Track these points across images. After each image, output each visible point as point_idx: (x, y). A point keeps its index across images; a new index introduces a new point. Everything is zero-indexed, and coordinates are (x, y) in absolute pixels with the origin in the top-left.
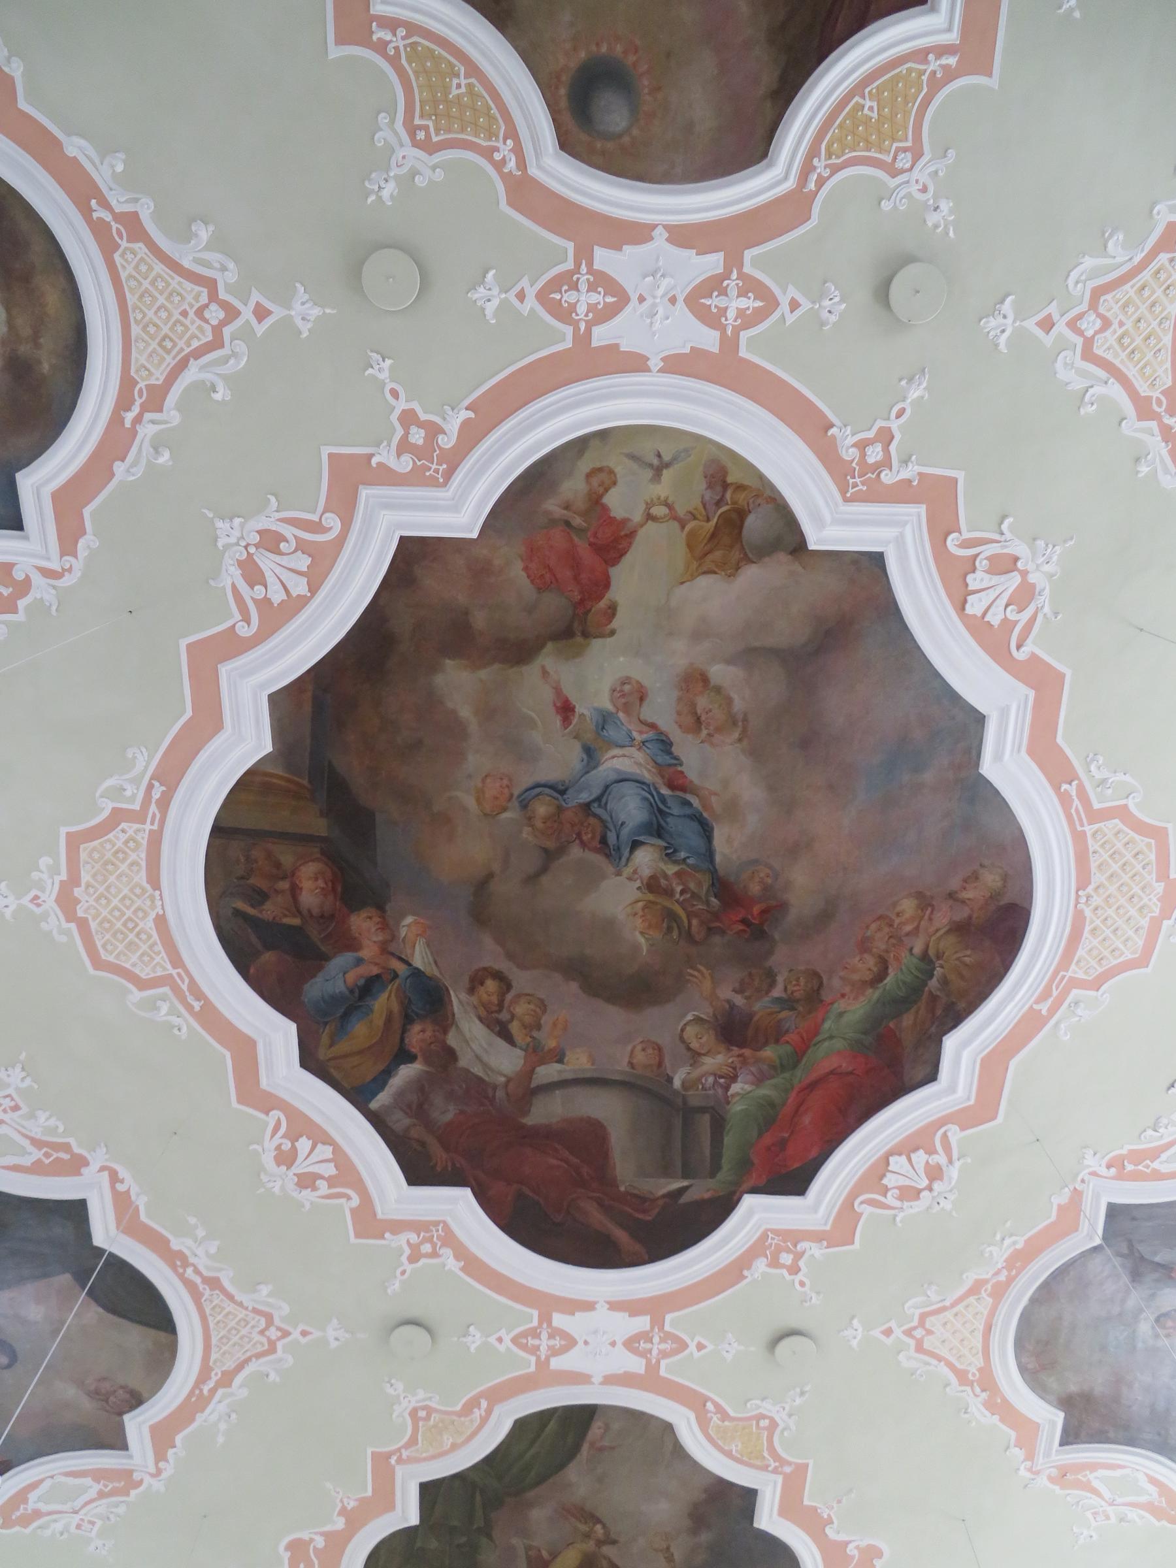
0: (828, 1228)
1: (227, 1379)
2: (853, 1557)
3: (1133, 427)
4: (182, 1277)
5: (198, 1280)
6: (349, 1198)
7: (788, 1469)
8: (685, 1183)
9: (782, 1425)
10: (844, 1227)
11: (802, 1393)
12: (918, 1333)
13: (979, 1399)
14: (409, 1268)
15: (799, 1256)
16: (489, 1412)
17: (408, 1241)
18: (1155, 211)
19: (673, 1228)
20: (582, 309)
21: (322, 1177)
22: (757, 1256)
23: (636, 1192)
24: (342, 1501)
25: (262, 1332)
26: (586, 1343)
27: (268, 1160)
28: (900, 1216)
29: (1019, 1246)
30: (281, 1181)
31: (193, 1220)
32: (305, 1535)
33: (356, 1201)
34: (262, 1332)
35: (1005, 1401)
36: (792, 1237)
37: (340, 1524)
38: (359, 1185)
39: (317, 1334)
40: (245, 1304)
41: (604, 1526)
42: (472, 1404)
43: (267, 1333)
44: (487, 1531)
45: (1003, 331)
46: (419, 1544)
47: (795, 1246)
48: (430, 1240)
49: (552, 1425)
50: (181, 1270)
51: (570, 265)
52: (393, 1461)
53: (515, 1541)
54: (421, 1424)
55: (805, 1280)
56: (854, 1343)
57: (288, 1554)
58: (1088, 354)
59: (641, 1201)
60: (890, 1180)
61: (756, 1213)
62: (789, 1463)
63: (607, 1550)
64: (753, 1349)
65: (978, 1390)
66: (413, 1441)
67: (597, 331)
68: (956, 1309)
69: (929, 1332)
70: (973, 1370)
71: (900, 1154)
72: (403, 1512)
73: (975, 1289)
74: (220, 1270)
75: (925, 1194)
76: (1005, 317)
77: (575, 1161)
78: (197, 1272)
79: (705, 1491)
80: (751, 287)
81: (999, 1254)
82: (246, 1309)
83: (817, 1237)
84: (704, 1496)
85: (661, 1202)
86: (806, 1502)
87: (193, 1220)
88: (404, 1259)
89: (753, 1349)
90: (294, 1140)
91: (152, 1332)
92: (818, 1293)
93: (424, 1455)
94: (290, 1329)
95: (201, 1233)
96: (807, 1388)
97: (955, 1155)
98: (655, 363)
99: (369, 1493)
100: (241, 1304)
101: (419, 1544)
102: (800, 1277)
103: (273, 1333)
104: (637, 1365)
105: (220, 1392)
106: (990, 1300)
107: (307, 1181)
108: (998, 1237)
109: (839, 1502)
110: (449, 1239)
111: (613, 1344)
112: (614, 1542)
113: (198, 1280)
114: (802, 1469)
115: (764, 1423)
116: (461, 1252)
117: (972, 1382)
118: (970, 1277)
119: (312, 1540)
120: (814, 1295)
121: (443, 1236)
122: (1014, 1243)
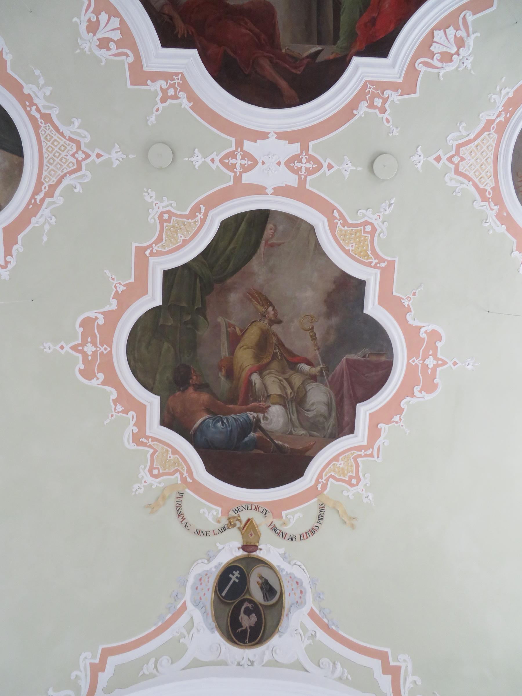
0: (401, 80)
1: (50, 194)
2: (424, 339)
3: (479, 204)
4: (28, 113)
5: (38, 116)
6: (128, 56)
7: (383, 265)
8: (319, 48)
9: (379, 230)
10: (409, 83)
11: (390, 205)
12: (456, 159)
13: (493, 212)
14: (161, 106)
15: (385, 101)
16: (206, 215)
17: (161, 87)
18: (481, 115)
19: (311, 82)
20: (238, 166)
21: (113, 41)
22: (360, 101)
23: (290, 53)
24: (116, 287)
25: (73, 155)
26: (263, 163)
27: (83, 28)
28: (442, 72)
29: (511, 95)
30: (88, 43)
31: (37, 72)
32: (92, 314)
33: (131, 59)
34: (73, 155)
35: (508, 214)
36: (382, 86)
37: (114, 305)
38: (134, 47)
39: (106, 156)
40: (65, 134)
41: (274, 309)
42: (196, 209)
43: (76, 155)
44: (202, 311)
45: (419, 162)
46: (161, 322)
47: (383, 94)
48: (173, 86)
49: (243, 226)
50: (28, 109)
51: (233, 148)
52: (147, 253)
53: (220, 319)
54: (165, 224)
55: (389, 118)
56: (419, 166)
57: (82, 329)
58: (457, 172)
59: (295, 59)
60: (435, 48)
61: (362, 70)
62: (384, 261)
63: (275, 328)
64: (360, 169)
65: (492, 204)
66: (160, 239)
67: (244, 176)
68: (477, 142)
69: (463, 159)
70: (488, 189)
71: (440, 30)
72: (152, 295)
73: (486, 128)
74: (51, 108)
75: (455, 57)
76: (420, 156)
77: (256, 30)
78: (38, 110)
79: (335, 282)
80: (311, 159)
81: (499, 100)
82: (65, 137)
83: (394, 86)
84: (333, 287)
85: (305, 61)
86: (395, 294)
87: (37, 72)
88: (158, 99)
89: (360, 169)
90: (98, 14)
91: (9, 155)
92: (397, 128)
93: (167, 249)
94: (89, 152)
95: (42, 81)
96: (393, 201)
97: (471, 31)
98: (270, 191)
99: (132, 280)
100: (62, 134)
101: (161, 322)
102: (386, 115)
103: (80, 156)
104: (292, 180)
105: (47, 200)
106: (496, 136)
107: (104, 44)
108: (498, 89)
109: (414, 294)
110: (185, 86)
111: (279, 164)
112: (280, 322)
113: (38, 116)
114: (391, 264)
115: (368, 228)
116: (192, 97)
117: (489, 198)
118: (484, 117)
119: (96, 318)
120: (395, 128)
121: (180, 83)
122: (508, 93)
